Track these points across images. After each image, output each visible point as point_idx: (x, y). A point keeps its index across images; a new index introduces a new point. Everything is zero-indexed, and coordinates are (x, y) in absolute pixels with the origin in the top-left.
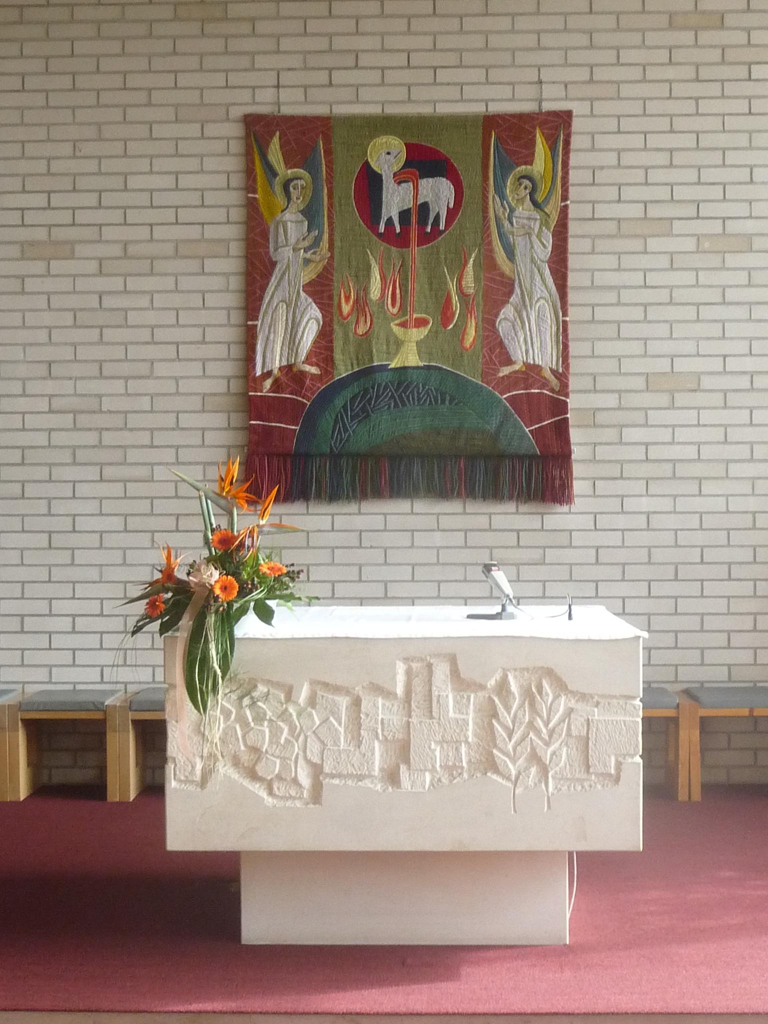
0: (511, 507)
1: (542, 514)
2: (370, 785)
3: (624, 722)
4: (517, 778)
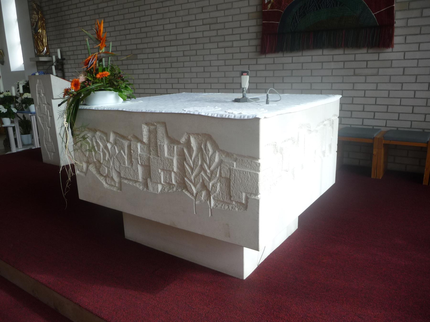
0: (364, 50)
1: (379, 53)
2: (138, 186)
3: (250, 173)
4: (197, 194)
